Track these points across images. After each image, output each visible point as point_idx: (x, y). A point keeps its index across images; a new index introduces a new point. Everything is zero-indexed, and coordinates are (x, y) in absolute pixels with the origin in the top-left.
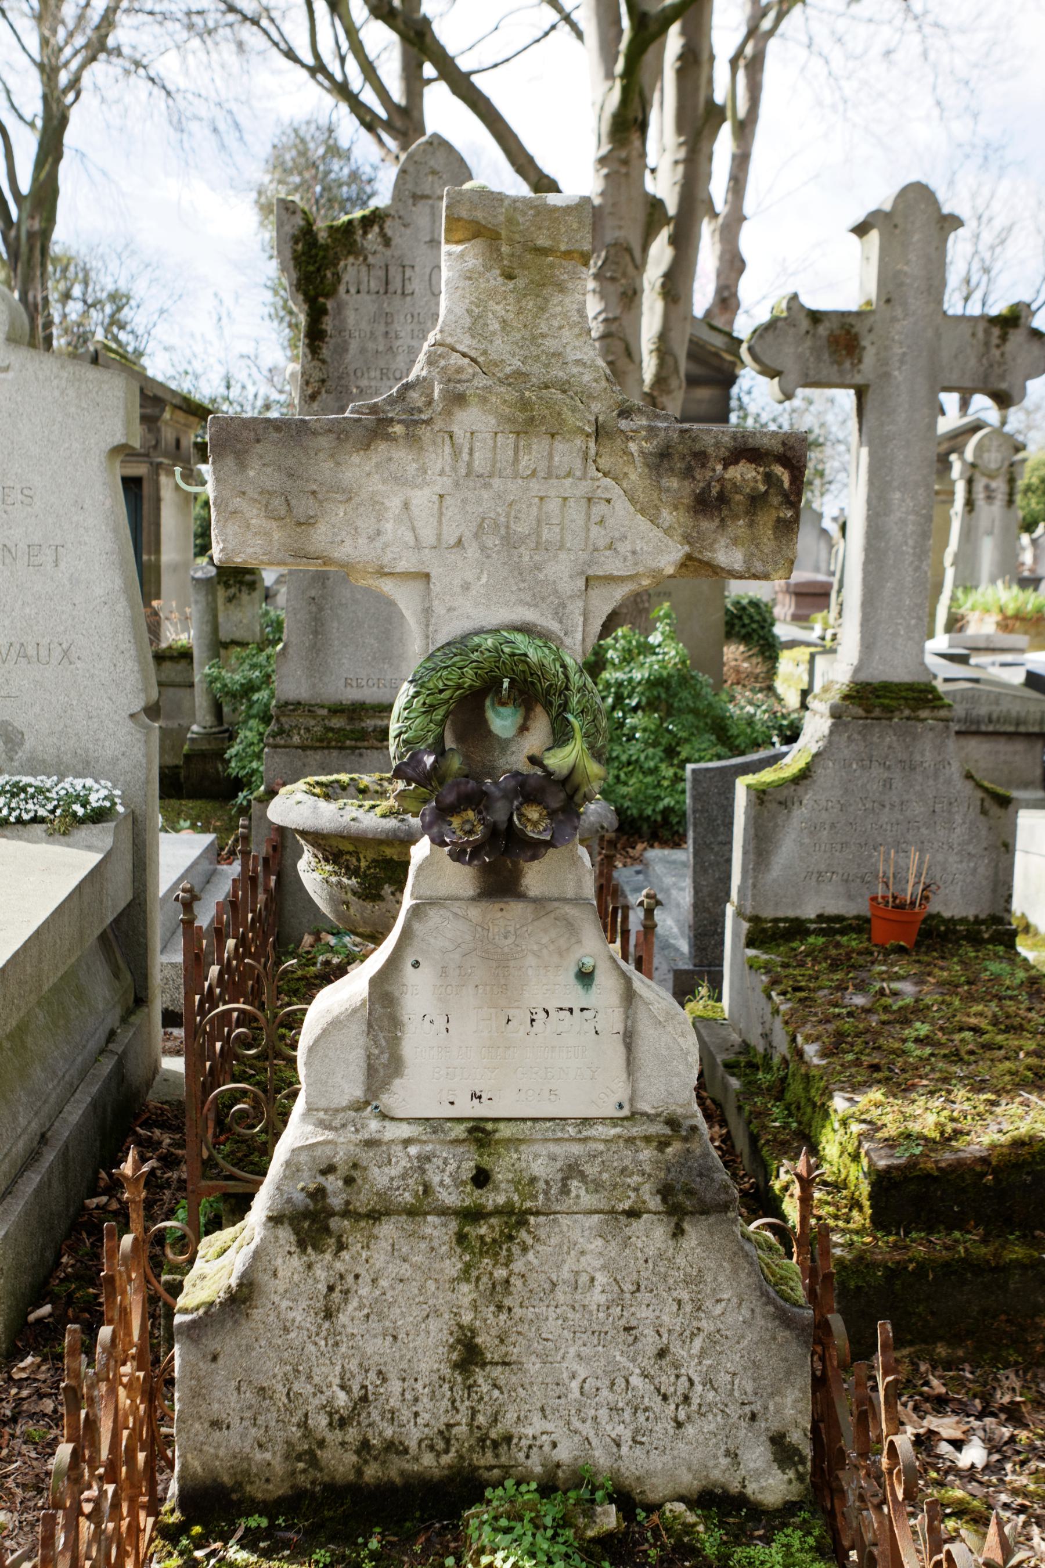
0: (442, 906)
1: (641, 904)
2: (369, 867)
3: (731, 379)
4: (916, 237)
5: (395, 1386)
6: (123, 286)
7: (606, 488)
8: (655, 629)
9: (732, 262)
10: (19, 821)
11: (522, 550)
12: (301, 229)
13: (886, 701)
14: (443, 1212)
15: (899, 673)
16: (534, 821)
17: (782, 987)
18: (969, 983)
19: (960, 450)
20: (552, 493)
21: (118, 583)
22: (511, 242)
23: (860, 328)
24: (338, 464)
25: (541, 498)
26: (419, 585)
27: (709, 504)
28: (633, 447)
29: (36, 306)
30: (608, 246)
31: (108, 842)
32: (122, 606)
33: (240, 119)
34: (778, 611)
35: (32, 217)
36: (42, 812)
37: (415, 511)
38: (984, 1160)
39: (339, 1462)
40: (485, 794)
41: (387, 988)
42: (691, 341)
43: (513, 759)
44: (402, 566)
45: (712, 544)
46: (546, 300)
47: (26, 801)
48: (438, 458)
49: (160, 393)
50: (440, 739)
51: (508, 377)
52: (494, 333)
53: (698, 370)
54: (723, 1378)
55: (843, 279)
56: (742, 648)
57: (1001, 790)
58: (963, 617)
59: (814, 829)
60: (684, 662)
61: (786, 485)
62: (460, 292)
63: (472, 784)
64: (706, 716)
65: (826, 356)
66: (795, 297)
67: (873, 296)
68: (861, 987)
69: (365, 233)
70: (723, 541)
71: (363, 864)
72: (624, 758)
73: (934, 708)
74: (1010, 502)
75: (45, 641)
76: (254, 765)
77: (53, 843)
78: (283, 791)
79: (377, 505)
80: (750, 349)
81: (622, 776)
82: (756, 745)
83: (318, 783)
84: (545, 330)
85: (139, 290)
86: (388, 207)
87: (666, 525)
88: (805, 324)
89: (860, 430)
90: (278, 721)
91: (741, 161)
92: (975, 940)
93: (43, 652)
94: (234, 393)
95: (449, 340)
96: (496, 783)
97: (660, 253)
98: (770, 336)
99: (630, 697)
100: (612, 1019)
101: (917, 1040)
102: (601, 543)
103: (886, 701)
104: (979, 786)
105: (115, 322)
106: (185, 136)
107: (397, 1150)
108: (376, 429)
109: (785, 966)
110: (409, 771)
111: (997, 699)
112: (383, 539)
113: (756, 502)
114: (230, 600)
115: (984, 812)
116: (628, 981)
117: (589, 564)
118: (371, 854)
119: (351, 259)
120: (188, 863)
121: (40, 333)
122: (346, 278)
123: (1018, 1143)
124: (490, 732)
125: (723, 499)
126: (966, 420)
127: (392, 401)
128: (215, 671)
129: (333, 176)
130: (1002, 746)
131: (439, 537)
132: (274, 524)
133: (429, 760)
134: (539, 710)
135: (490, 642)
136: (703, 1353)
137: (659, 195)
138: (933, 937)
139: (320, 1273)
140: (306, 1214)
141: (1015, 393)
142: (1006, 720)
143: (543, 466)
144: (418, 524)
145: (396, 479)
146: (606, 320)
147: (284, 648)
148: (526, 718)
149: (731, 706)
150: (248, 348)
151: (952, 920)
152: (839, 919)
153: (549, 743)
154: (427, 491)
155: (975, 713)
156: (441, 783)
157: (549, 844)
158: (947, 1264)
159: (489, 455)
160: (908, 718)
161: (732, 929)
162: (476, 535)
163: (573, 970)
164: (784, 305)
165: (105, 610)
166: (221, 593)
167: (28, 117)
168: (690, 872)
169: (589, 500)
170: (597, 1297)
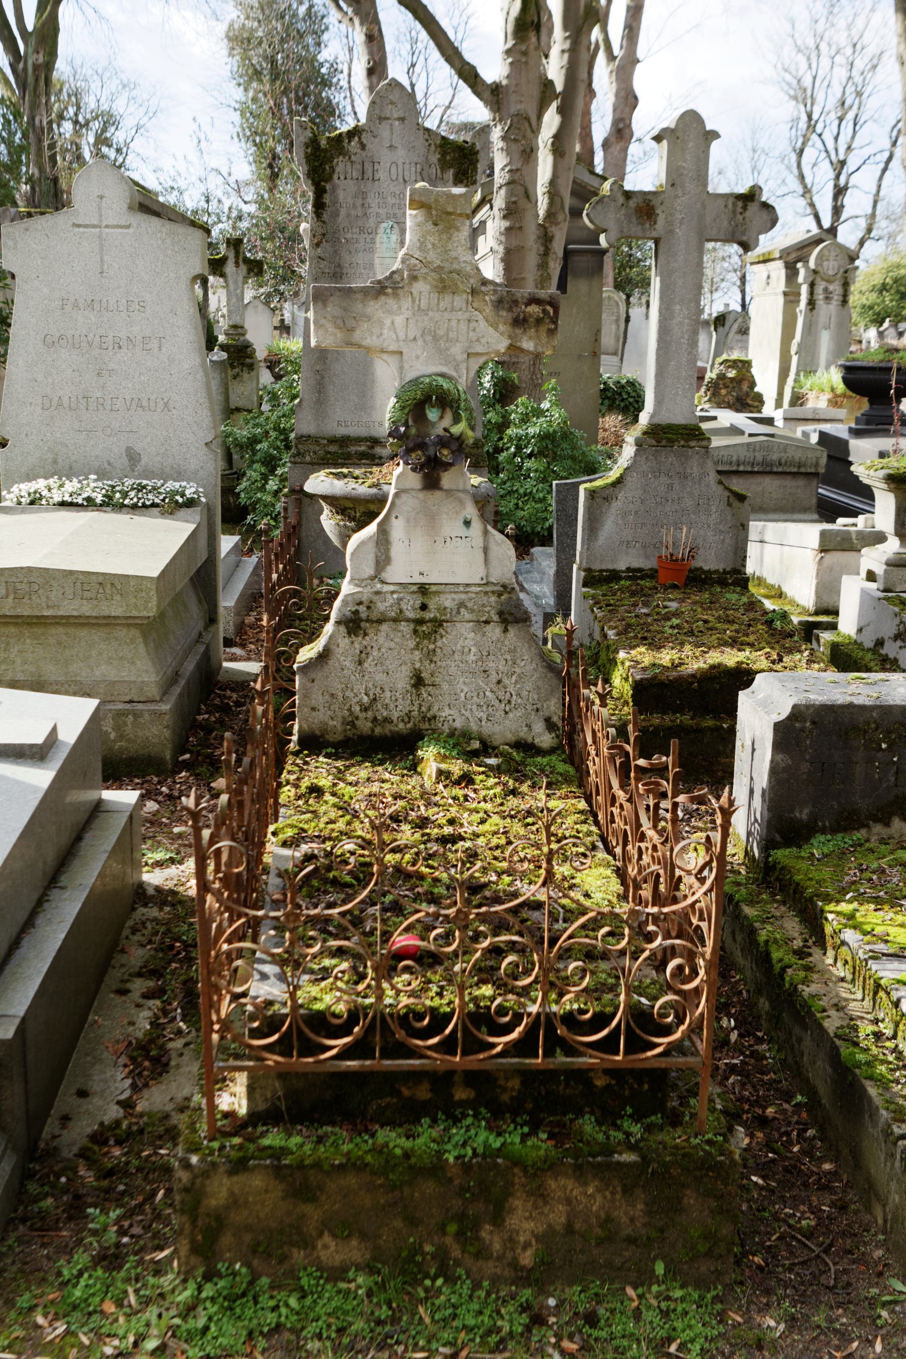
4: (691, 145)
5: (388, 694)
9: (626, 98)
14: (408, 620)
15: (678, 418)
19: (804, 259)
23: (655, 202)
27: (519, 322)
36: (157, 501)
38: (693, 676)
39: (364, 726)
42: (574, 182)
44: (391, 348)
48: (406, 303)
54: (525, 693)
59: (625, 514)
68: (646, 604)
72: (521, 491)
75: (153, 397)
76: (259, 495)
79: (381, 323)
85: (119, 107)
88: (621, 200)
92: (723, 583)
93: (152, 404)
94: (213, 206)
97: (551, 120)
100: (479, 541)
101: (672, 627)
107: (388, 596)
111: (785, 448)
113: (539, 321)
114: (235, 377)
115: (729, 505)
118: (362, 509)
122: (338, 170)
123: (713, 667)
125: (525, 320)
130: (789, 482)
133: (402, 429)
136: (516, 682)
138: (696, 580)
139: (357, 645)
140: (351, 620)
141: (752, 243)
152: (640, 570)
157: (451, 465)
158: (670, 728)
161: (576, 576)
166: (230, 373)
170: (472, 657)
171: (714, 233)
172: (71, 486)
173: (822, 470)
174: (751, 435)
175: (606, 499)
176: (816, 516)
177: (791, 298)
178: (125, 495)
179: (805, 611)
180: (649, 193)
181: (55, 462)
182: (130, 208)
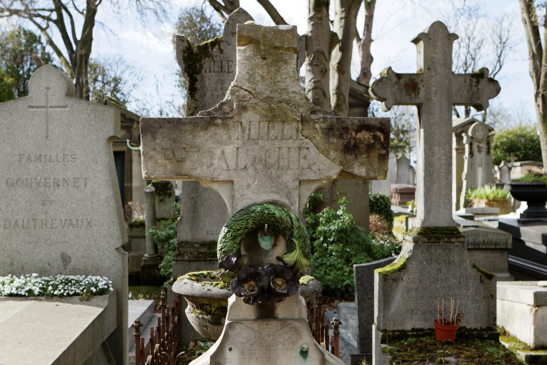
0: (241, 323)
1: (333, 323)
2: (215, 311)
3: (367, 105)
4: (439, 43)
6: (118, 75)
7: (307, 143)
8: (340, 208)
9: (367, 58)
10: (68, 295)
11: (272, 170)
12: (186, 47)
13: (437, 235)
15: (442, 223)
16: (280, 285)
17: (397, 360)
18: (479, 357)
20: (284, 146)
21: (111, 193)
22: (265, 45)
24: (194, 136)
25: (280, 148)
26: (229, 186)
28: (317, 126)
29: (83, 84)
30: (314, 52)
31: (106, 303)
32: (112, 203)
33: (165, 8)
34: (393, 201)
35: (82, 49)
36: (78, 291)
37: (227, 155)
40: (258, 274)
41: (218, 360)
42: (350, 89)
43: (270, 258)
44: (222, 178)
45: (352, 166)
46: (280, 68)
47: (71, 286)
48: (236, 133)
49: (132, 117)
50: (239, 251)
51: (264, 99)
52: (258, 81)
53: (353, 101)
55: (409, 61)
56: (377, 216)
57: (488, 272)
58: (471, 201)
59: (408, 291)
60: (352, 222)
61: (382, 140)
62: (244, 65)
63: (253, 269)
64: (362, 245)
65: (404, 92)
66: (390, 68)
67: (423, 68)
69: (213, 48)
70: (357, 164)
71: (213, 309)
72: (328, 263)
73: (457, 237)
74: (488, 152)
75: (80, 218)
77: (82, 304)
78: (179, 279)
79: (211, 153)
80: (372, 90)
81: (328, 271)
82: (384, 257)
83: (194, 275)
84: (279, 79)
85: (125, 77)
86: (222, 38)
87: (332, 158)
88: (395, 79)
89: (420, 122)
90: (178, 250)
91: (369, 19)
92: (481, 338)
93: (80, 223)
95: (240, 85)
96: (263, 269)
97: (336, 54)
98: (380, 85)
99: (330, 237)
102: (305, 166)
103: (437, 235)
104: (479, 270)
105: (115, 90)
106: (144, 16)
108: (210, 122)
109: (399, 351)
110: (225, 264)
112: (213, 167)
113: (370, 147)
114: (161, 201)
115: (482, 282)
116: (323, 355)
117: (300, 175)
119: (207, 59)
120: (142, 313)
121: (85, 95)
122: (205, 66)
124: (260, 247)
125: (356, 146)
126: (468, 119)
127: (216, 110)
128: (154, 231)
129: (203, 29)
130: (490, 254)
131: (237, 165)
132: (168, 162)
133: (234, 260)
134: (281, 237)
135: (259, 209)
137: (335, 31)
141: (484, 105)
142: (491, 243)
143: (279, 135)
144: (228, 160)
145: (218, 142)
146: (314, 82)
147: (181, 219)
148: (276, 241)
149: (373, 241)
150: (170, 99)
151: (470, 329)
153: (286, 251)
154: (231, 146)
155: (477, 240)
156: (239, 270)
157: (286, 295)
159: (257, 131)
160: (447, 242)
162: (252, 164)
163: (299, 350)
164: (386, 72)
165: (106, 205)
166: (157, 198)
167: (81, 11)
168: (356, 312)
169: (300, 148)
171: (458, 100)
172: (18, 282)
173: (510, 247)
174: (464, 227)
175: (395, 280)
176: (508, 275)
177: (460, 151)
178: (55, 287)
179: (526, 348)
180: (413, 74)
181: (12, 264)
182: (69, 95)
